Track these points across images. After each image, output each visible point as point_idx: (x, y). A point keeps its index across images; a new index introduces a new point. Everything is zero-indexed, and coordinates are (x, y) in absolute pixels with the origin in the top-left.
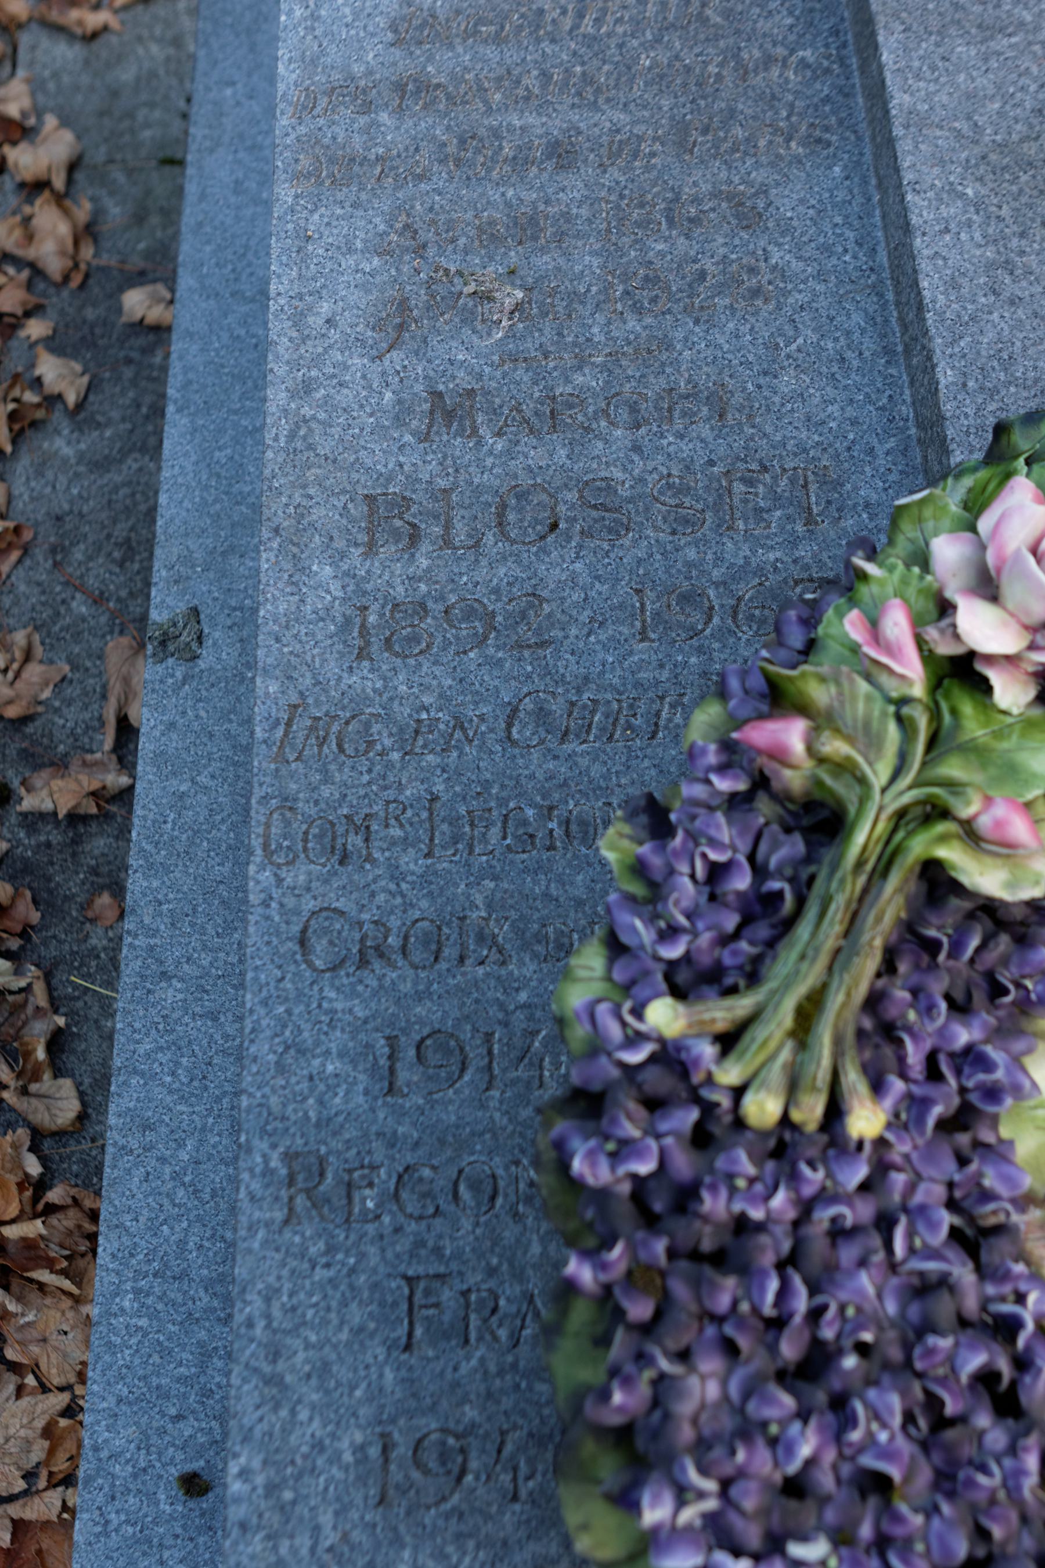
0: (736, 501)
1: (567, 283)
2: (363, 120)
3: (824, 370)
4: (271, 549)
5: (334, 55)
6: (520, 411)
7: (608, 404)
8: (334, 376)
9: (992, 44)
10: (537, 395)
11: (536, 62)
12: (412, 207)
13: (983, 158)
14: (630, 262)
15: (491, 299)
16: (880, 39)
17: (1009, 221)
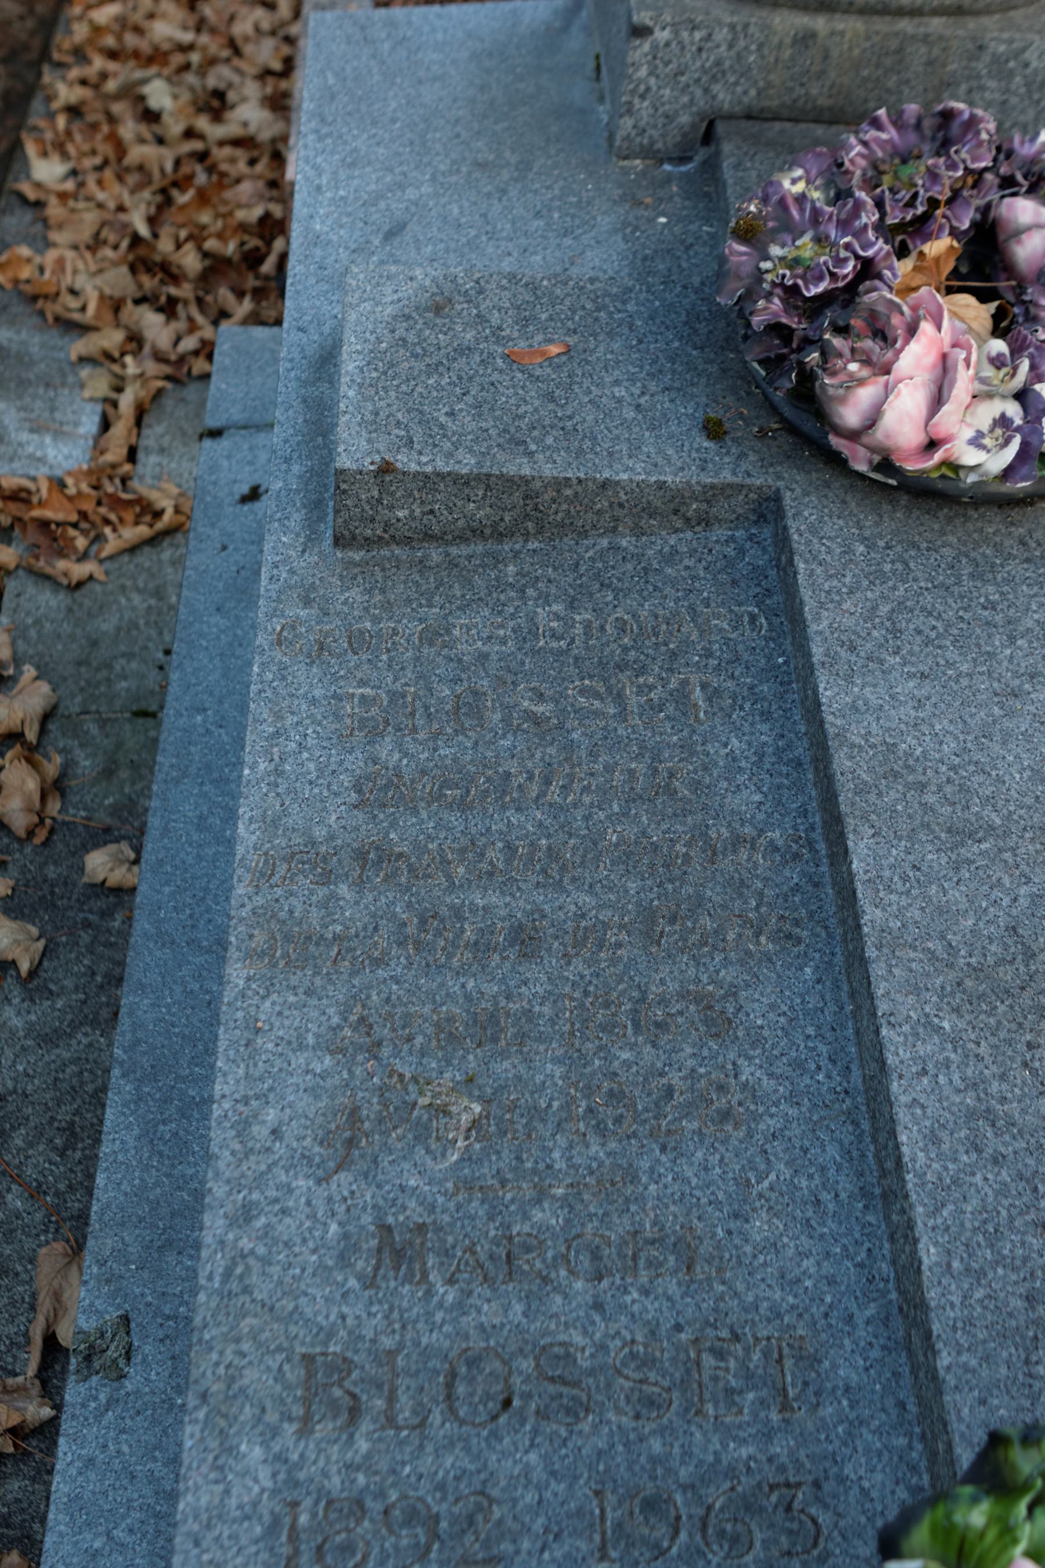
0: (705, 1378)
1: (527, 1096)
2: (322, 892)
3: (798, 1213)
4: (196, 1421)
5: (295, 817)
6: (474, 1253)
7: (569, 1248)
8: (276, 1200)
9: (963, 851)
10: (492, 1233)
11: (501, 833)
12: (368, 997)
13: (959, 984)
14: (594, 1073)
15: (446, 1113)
16: (850, 844)
17: (988, 1060)
